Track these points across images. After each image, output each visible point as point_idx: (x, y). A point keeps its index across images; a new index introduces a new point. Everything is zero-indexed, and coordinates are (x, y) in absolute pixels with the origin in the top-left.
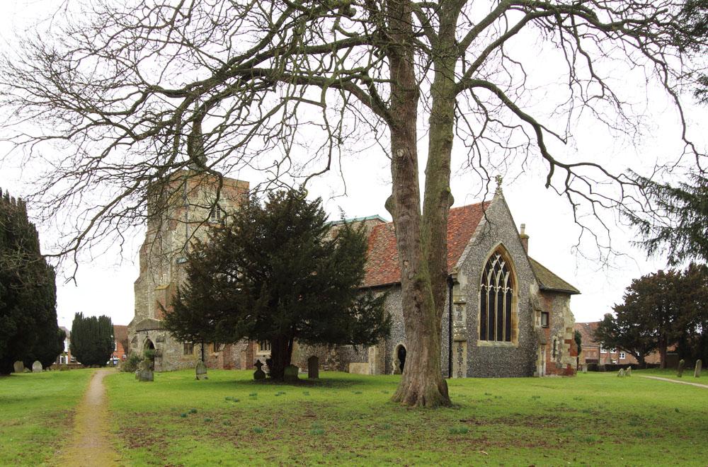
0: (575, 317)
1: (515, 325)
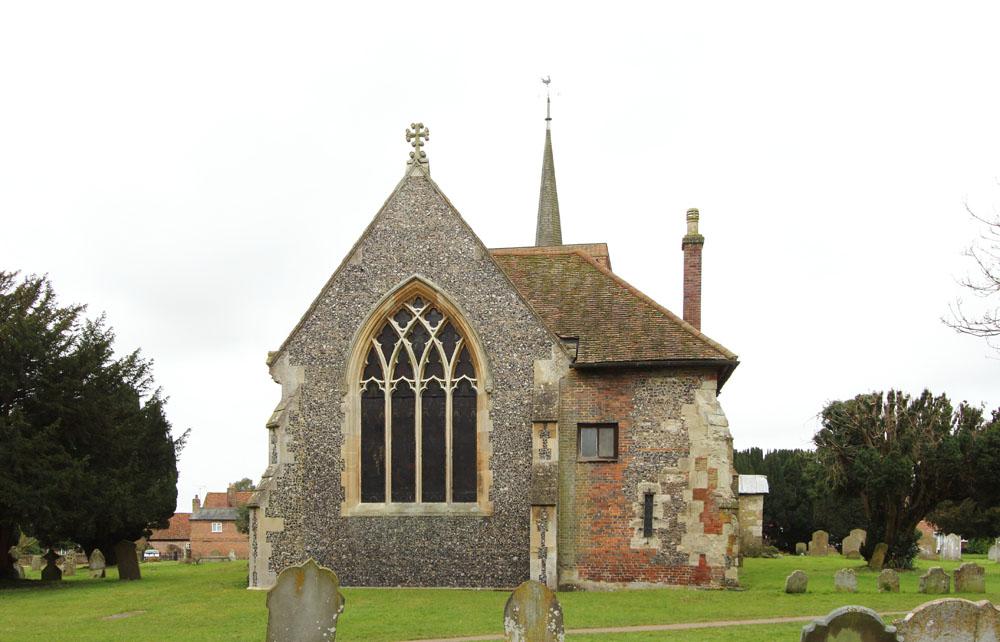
0: (240, 480)
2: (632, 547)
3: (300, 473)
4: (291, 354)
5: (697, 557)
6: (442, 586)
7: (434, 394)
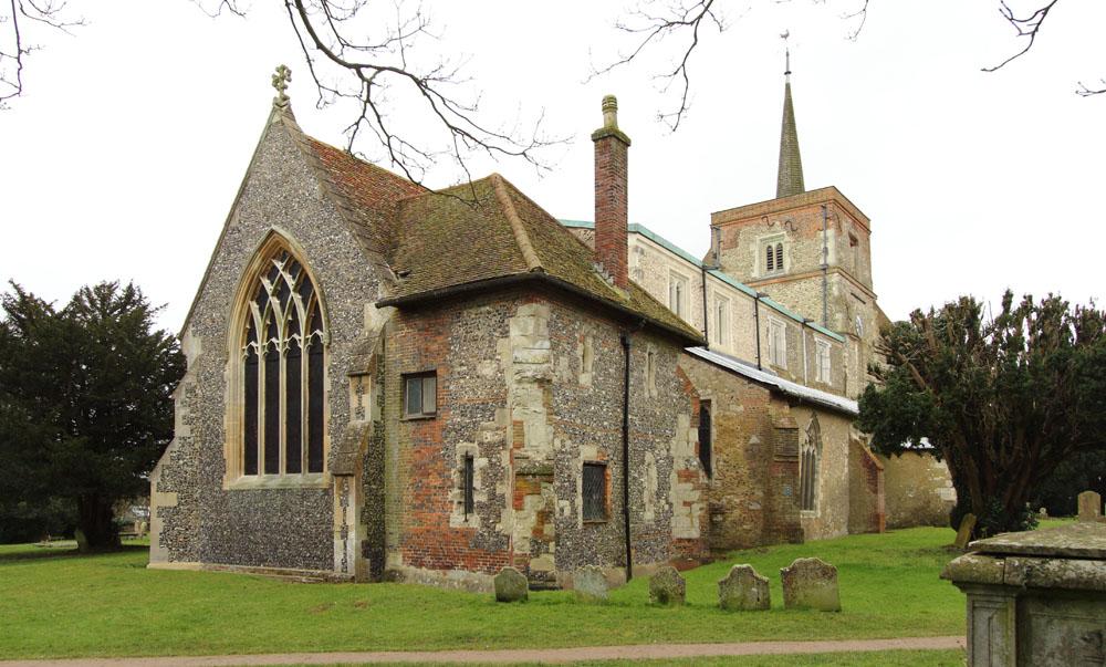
2: (451, 525)
3: (197, 446)
7: (293, 353)
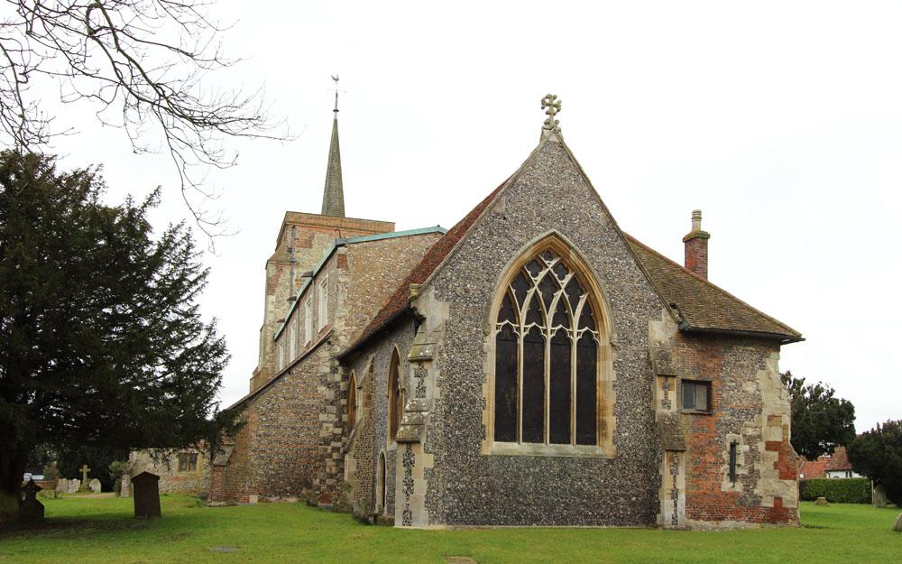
1: (605, 408)
4: (436, 289)
5: (771, 499)
6: (573, 524)
